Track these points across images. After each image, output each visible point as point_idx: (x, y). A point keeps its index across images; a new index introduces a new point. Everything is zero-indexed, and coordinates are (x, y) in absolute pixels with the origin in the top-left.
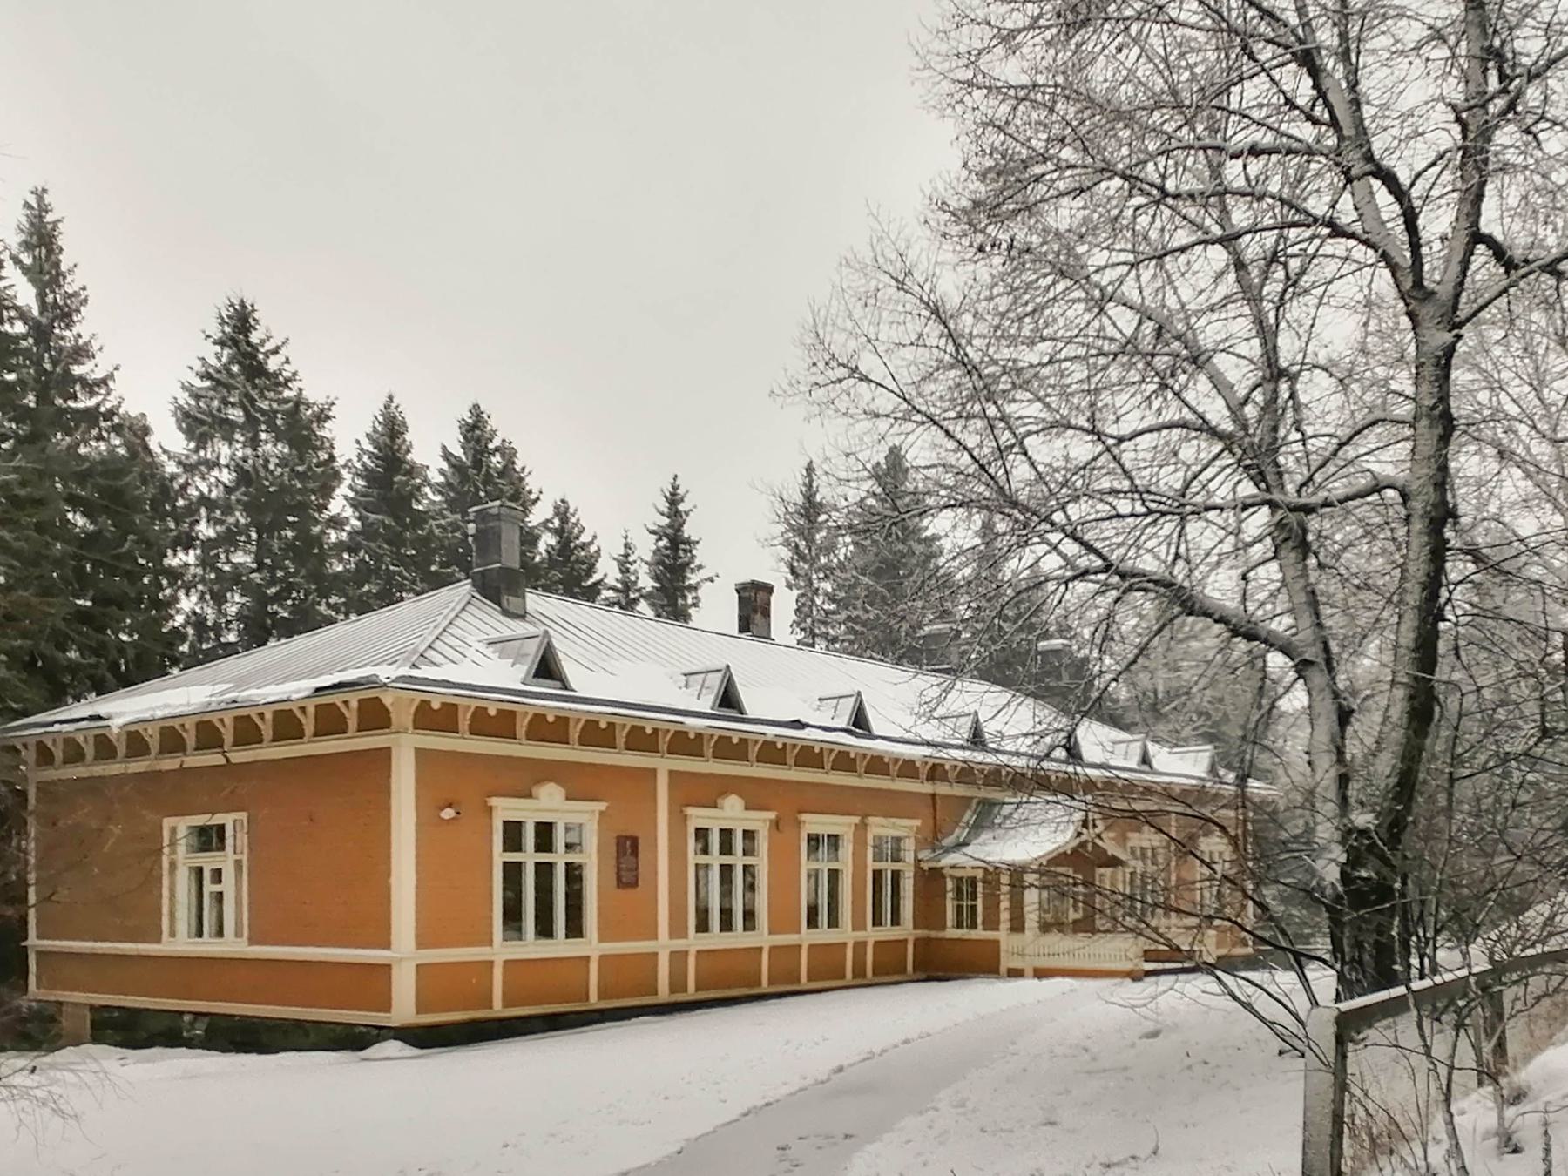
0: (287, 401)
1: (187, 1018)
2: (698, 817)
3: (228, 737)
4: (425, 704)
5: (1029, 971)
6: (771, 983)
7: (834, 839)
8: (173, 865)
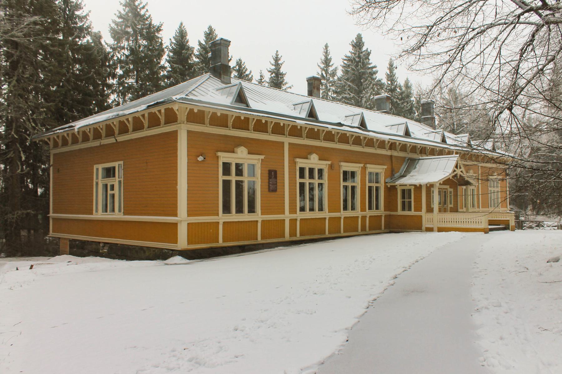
0: (147, 24)
1: (101, 245)
2: (301, 163)
3: (117, 132)
4: (191, 111)
5: (435, 229)
6: (329, 233)
7: (353, 174)
8: (97, 183)
